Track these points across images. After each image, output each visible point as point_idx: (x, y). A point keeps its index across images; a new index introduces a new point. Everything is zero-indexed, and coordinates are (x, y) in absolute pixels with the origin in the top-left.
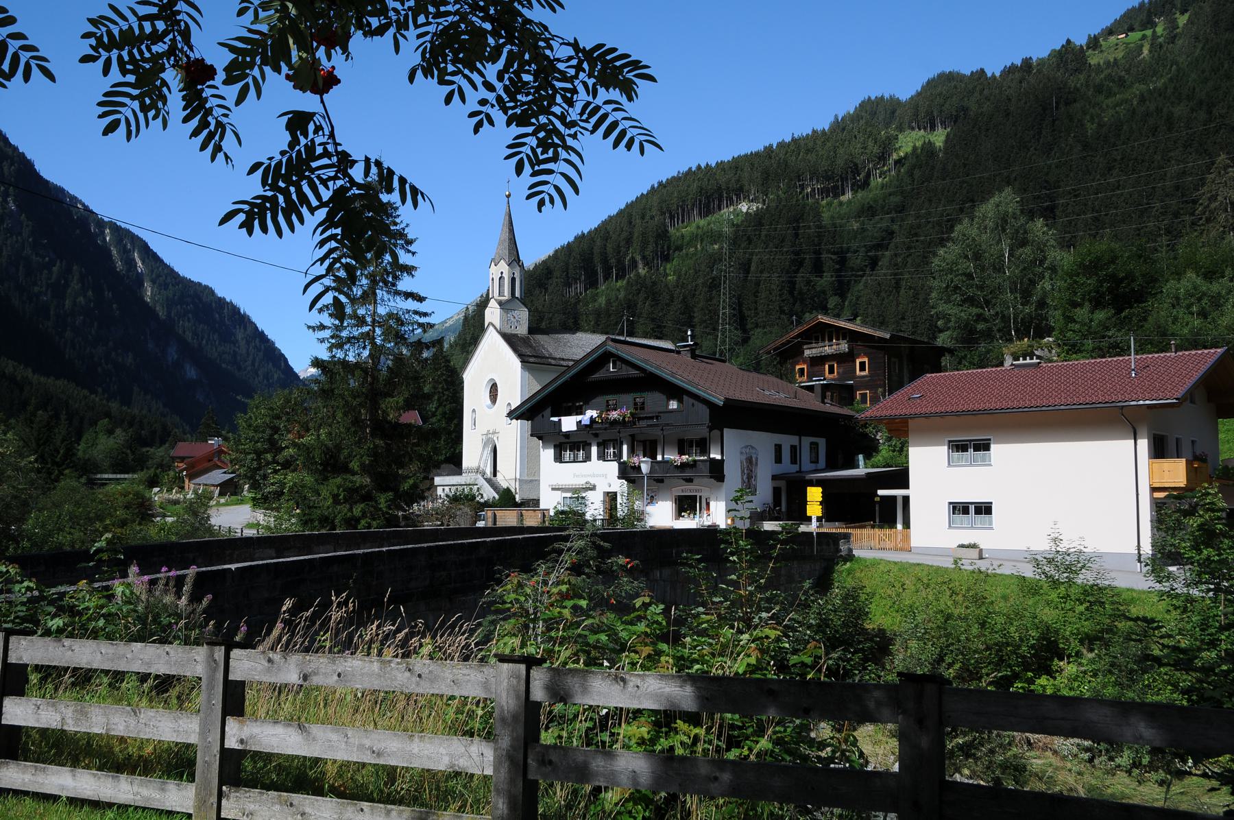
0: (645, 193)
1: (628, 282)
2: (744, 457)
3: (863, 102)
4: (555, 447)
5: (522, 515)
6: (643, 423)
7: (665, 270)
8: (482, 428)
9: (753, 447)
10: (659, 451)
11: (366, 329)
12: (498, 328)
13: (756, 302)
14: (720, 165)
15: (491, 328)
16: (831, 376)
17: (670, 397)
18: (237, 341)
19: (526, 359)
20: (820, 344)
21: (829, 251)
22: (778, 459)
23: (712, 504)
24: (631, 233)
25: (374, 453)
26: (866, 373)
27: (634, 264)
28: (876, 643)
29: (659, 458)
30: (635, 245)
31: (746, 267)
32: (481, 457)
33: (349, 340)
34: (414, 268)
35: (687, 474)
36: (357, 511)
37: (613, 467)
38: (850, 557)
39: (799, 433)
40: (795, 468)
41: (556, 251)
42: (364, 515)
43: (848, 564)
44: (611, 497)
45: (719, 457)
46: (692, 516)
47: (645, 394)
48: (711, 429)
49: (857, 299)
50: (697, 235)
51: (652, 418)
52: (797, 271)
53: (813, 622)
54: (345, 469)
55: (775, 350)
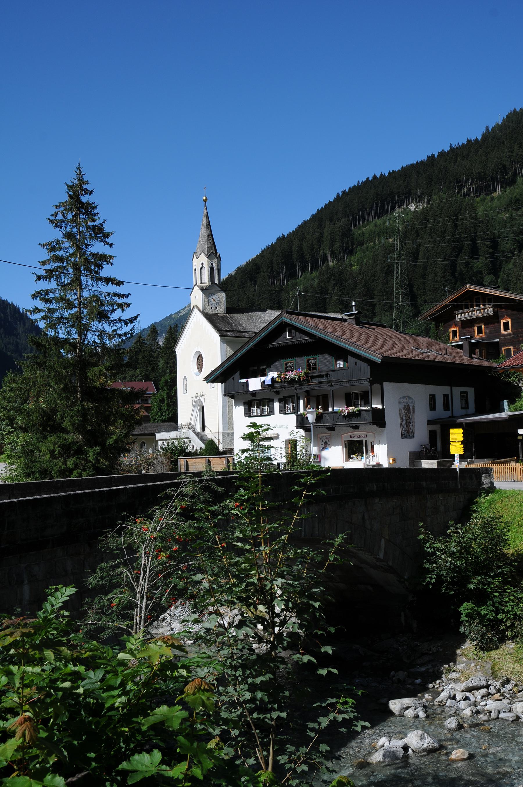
0: (332, 200)
1: (320, 272)
2: (402, 406)
3: (509, 114)
4: (245, 404)
5: (209, 461)
6: (315, 381)
7: (350, 261)
8: (192, 391)
9: (409, 398)
10: (330, 404)
11: (75, 310)
12: (201, 309)
13: (424, 283)
14: (392, 174)
15: (196, 310)
16: (480, 336)
17: (337, 358)
18: (19, 334)
19: (224, 333)
20: (470, 310)
21: (483, 239)
22: (433, 406)
23: (376, 447)
24: (322, 234)
25: (84, 413)
26: (510, 331)
27: (325, 258)
28: (514, 567)
29: (330, 410)
30: (325, 243)
31: (415, 255)
32: (192, 415)
33: (61, 319)
34: (111, 257)
35: (354, 422)
36: (70, 463)
37: (292, 419)
38: (492, 489)
39: (450, 384)
40: (448, 413)
41: (263, 251)
42: (76, 466)
43: (490, 496)
44: (292, 444)
45: (380, 407)
46: (359, 457)
47: (316, 357)
48: (372, 383)
49: (508, 276)
50: (375, 232)
51: (322, 376)
52: (458, 256)
53: (455, 550)
54: (58, 429)
55: (430, 316)
